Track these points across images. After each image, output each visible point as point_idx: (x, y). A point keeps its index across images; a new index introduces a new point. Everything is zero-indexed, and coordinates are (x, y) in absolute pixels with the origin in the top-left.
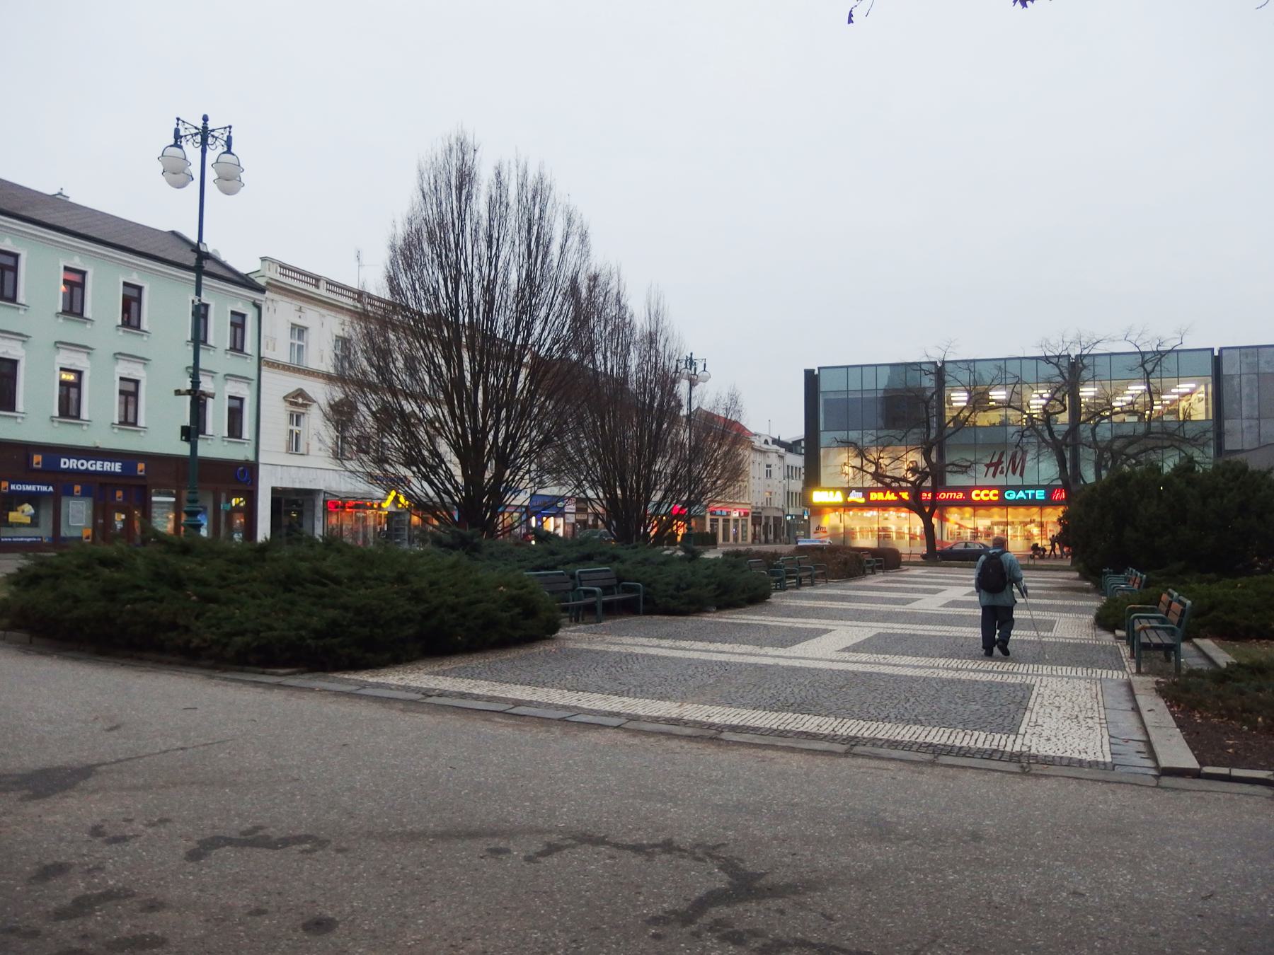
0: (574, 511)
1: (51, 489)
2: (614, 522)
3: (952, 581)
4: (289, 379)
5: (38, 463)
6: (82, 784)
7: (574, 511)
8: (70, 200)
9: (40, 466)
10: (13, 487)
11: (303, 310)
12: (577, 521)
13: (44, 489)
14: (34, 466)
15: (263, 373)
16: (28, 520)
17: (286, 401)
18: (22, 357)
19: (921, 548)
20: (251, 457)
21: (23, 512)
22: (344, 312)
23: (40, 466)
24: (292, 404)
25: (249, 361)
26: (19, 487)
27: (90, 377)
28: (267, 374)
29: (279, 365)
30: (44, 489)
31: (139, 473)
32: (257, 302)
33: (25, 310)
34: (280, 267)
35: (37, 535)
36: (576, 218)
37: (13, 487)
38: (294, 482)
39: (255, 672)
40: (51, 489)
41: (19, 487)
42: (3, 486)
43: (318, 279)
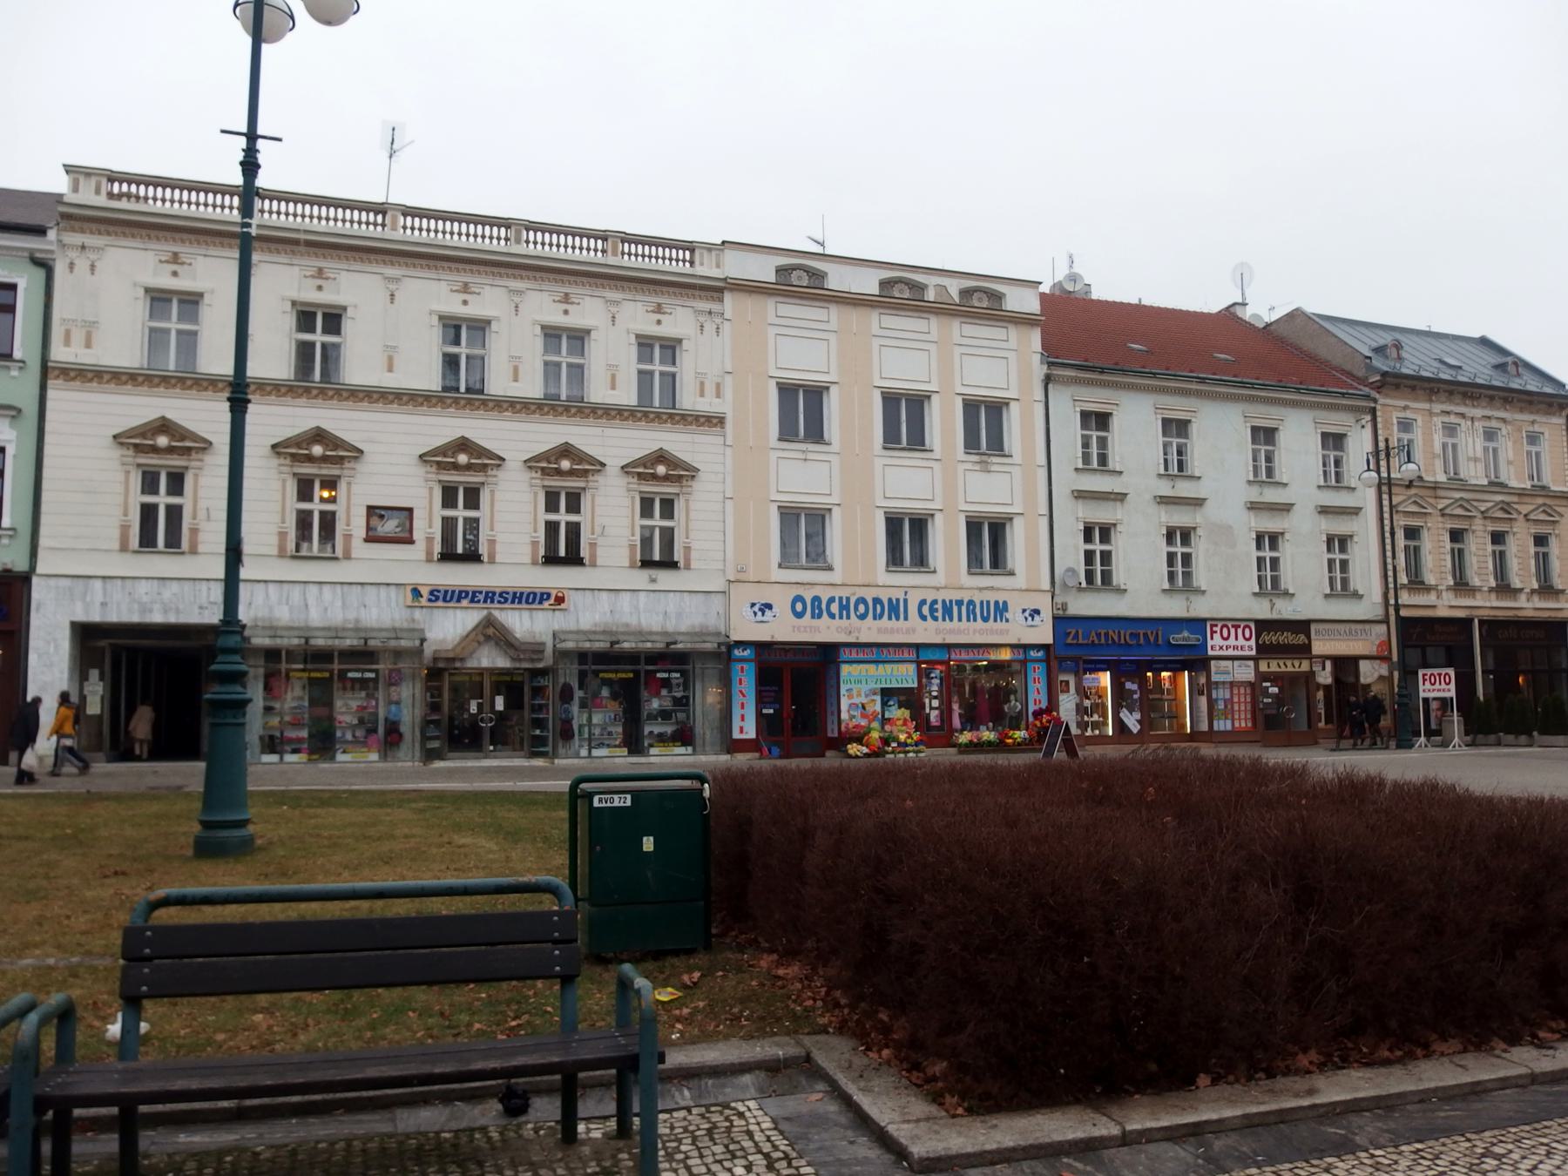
0: (1253, 653)
4: (423, 419)
6: (781, 1053)
7: (1253, 653)
8: (1096, 294)
11: (183, 258)
12: (1262, 677)
15: (51, 394)
17: (278, 454)
18: (9, 441)
20: (21, 565)
22: (302, 248)
24: (441, 466)
25: (14, 373)
27: (15, 456)
28: (60, 397)
29: (697, 418)
32: (38, 255)
33: (21, 368)
34: (405, 215)
38: (144, 609)
43: (690, 247)
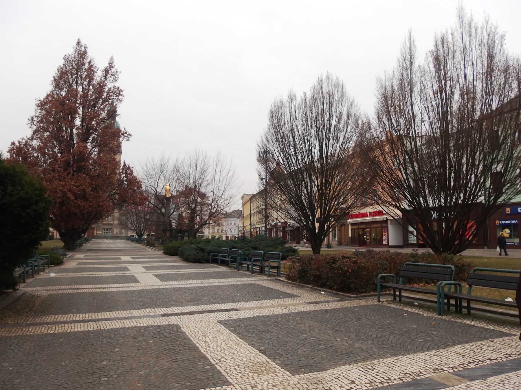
1: (517, 221)
2: (411, 229)
3: (148, 260)
5: (508, 212)
9: (509, 213)
10: (500, 222)
13: (514, 222)
14: (507, 213)
16: (508, 236)
19: (463, 300)
21: (505, 232)
23: (509, 213)
26: (503, 222)
30: (514, 222)
31: (507, 213)
35: (512, 242)
36: (330, 77)
37: (500, 222)
39: (414, 294)
40: (517, 221)
41: (503, 222)
42: (497, 222)
